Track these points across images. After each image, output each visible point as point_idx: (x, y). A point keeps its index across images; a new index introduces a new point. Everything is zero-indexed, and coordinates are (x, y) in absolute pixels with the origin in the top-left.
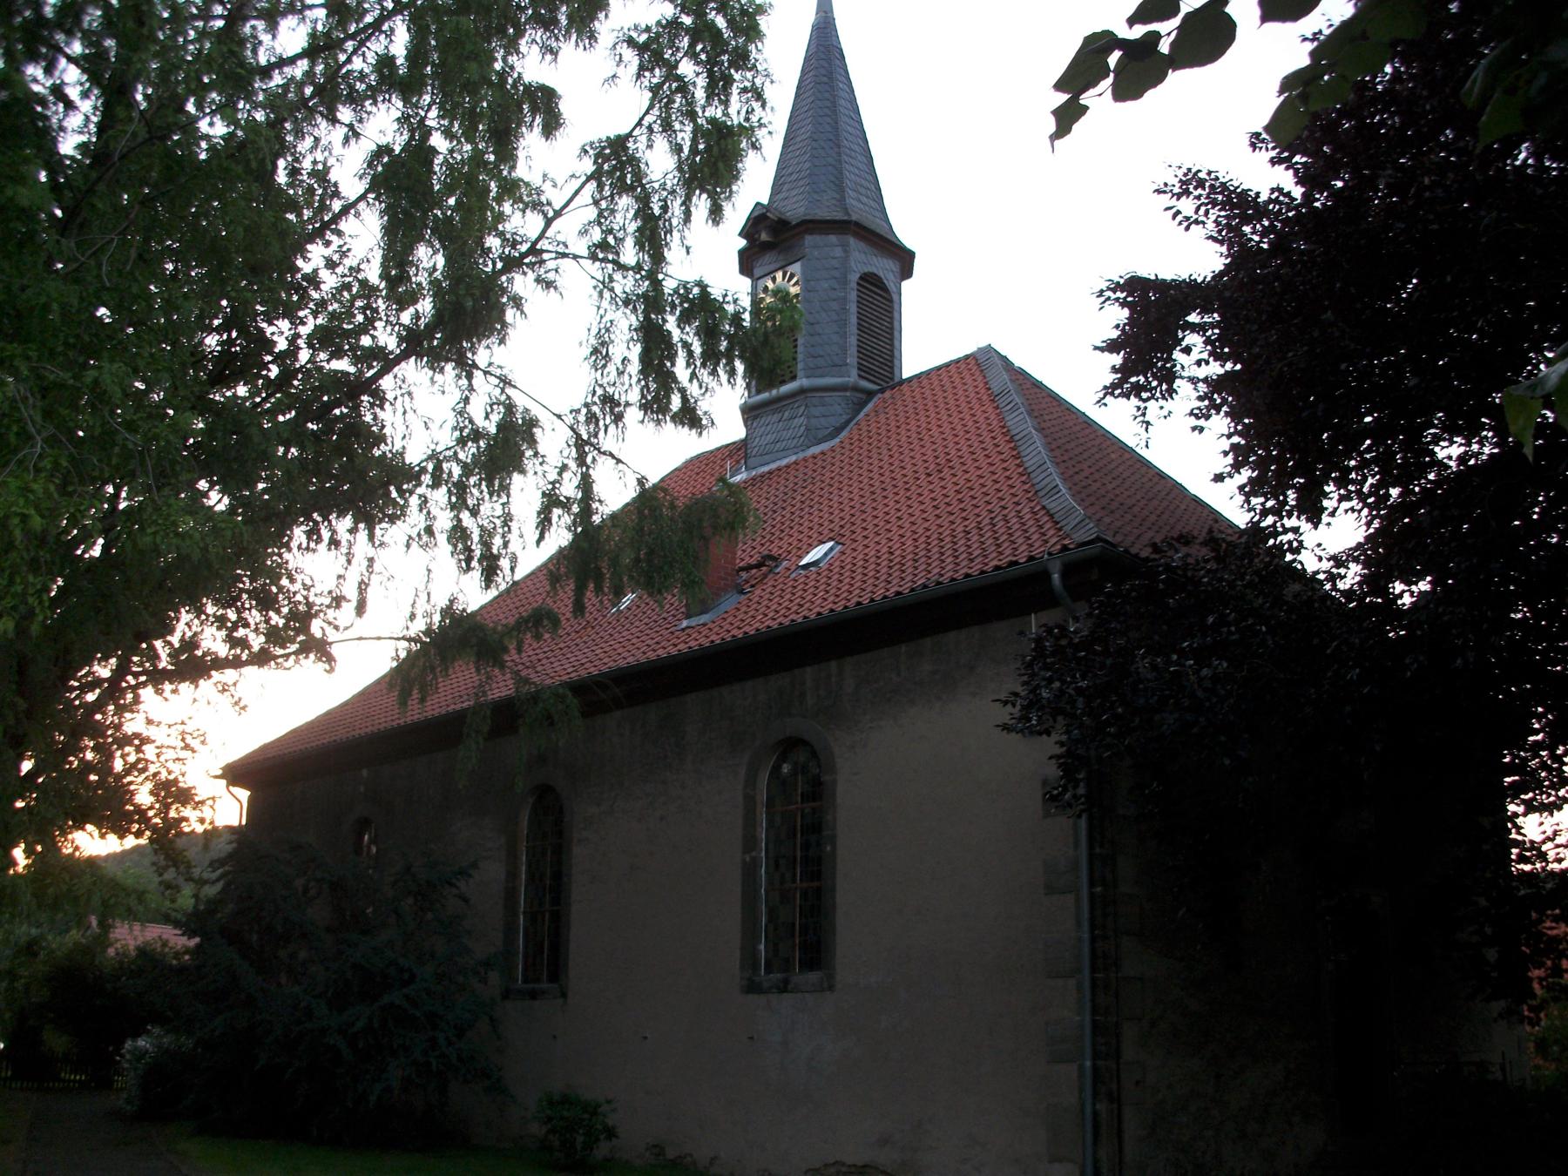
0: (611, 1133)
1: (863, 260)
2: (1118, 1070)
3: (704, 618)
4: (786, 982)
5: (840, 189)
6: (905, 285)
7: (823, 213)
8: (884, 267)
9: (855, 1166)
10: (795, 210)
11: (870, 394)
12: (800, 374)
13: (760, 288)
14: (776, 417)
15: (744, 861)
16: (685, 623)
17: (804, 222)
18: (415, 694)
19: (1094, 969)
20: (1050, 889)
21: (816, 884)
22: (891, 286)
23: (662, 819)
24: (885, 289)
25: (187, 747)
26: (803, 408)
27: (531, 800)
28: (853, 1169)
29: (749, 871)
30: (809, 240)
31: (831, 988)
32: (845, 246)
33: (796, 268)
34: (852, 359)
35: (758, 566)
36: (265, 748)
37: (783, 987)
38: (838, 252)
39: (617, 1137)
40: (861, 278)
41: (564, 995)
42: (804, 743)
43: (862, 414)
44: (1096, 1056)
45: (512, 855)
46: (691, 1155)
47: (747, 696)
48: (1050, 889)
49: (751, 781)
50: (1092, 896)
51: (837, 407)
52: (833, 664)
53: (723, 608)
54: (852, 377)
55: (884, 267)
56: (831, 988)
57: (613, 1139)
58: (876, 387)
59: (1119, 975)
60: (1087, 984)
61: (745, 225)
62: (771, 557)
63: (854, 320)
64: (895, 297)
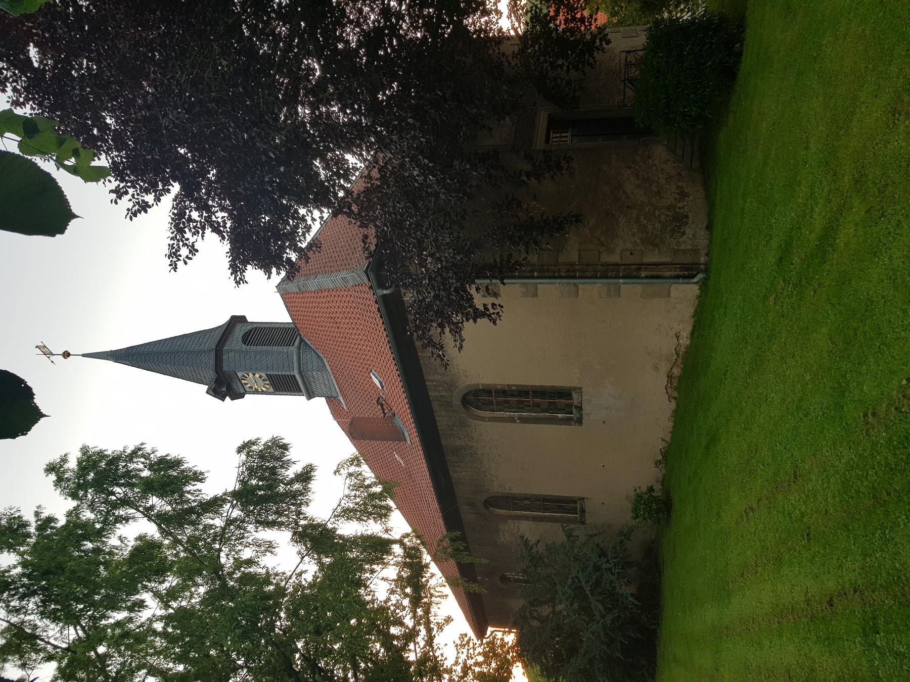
0: (651, 489)
1: (235, 341)
2: (625, 265)
3: (406, 435)
4: (576, 407)
5: (200, 352)
6: (249, 320)
7: (212, 361)
8: (239, 331)
10: (211, 374)
11: (302, 340)
12: (292, 373)
13: (250, 390)
14: (313, 384)
15: (519, 423)
16: (409, 442)
17: (216, 371)
19: (574, 277)
20: (535, 295)
21: (531, 393)
22: (249, 327)
23: (499, 456)
24: (251, 331)
25: (468, 642)
26: (309, 373)
27: (491, 509)
28: (669, 381)
29: (524, 420)
30: (225, 369)
31: (580, 389)
32: (229, 351)
33: (240, 374)
34: (285, 349)
35: (382, 405)
36: (467, 619)
37: (580, 408)
38: (232, 355)
39: (653, 486)
40: (245, 344)
41: (583, 499)
43: (312, 346)
44: (618, 277)
45: (518, 518)
46: (661, 449)
47: (443, 419)
48: (535, 295)
49: (483, 419)
50: (538, 278)
51: (307, 357)
52: (427, 383)
53: (401, 425)
54: (293, 349)
55: (239, 331)
56: (580, 389)
57: (654, 488)
59: (577, 263)
60: (583, 281)
61: (261, 323)
62: (377, 401)
63: (265, 348)
64: (254, 326)
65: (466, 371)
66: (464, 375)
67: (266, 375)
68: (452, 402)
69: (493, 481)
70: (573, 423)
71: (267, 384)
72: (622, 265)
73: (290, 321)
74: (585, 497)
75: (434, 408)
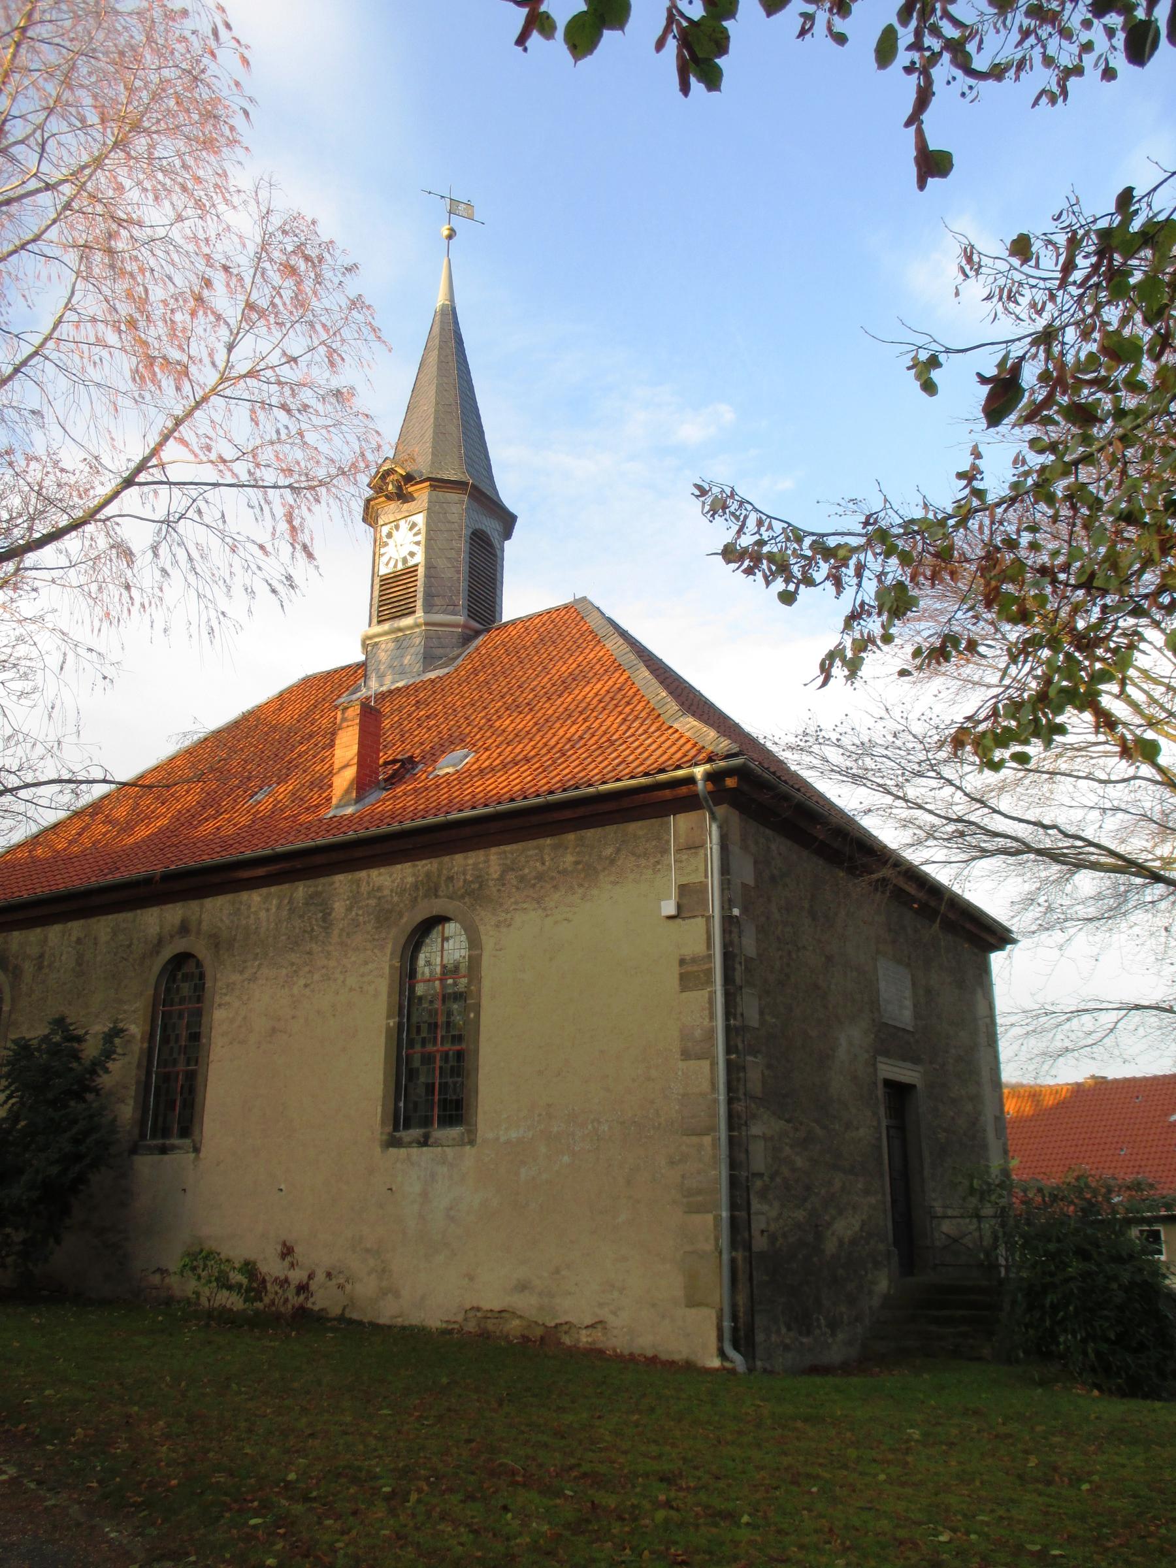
6: (507, 544)
8: (491, 526)
9: (491, 1311)
18: (1005, 505)
20: (686, 1055)
22: (496, 543)
23: (306, 986)
24: (491, 545)
31: (472, 1142)
41: (197, 1150)
42: (193, 956)
55: (491, 526)
58: (482, 627)
64: (498, 553)
65: (509, 925)
66: (499, 922)
67: (416, 565)
68: (437, 896)
69: (241, 972)
70: (390, 1129)
71: (395, 566)
72: (749, 1214)
73: (505, 619)
74: (202, 1155)
75: (470, 854)
